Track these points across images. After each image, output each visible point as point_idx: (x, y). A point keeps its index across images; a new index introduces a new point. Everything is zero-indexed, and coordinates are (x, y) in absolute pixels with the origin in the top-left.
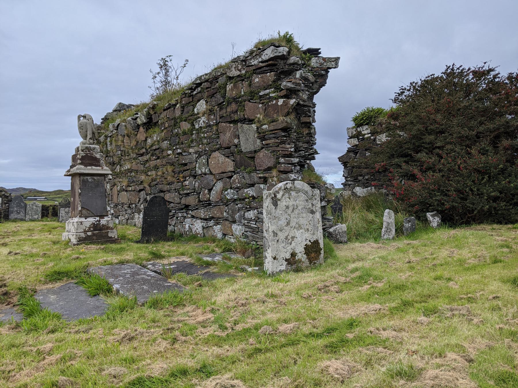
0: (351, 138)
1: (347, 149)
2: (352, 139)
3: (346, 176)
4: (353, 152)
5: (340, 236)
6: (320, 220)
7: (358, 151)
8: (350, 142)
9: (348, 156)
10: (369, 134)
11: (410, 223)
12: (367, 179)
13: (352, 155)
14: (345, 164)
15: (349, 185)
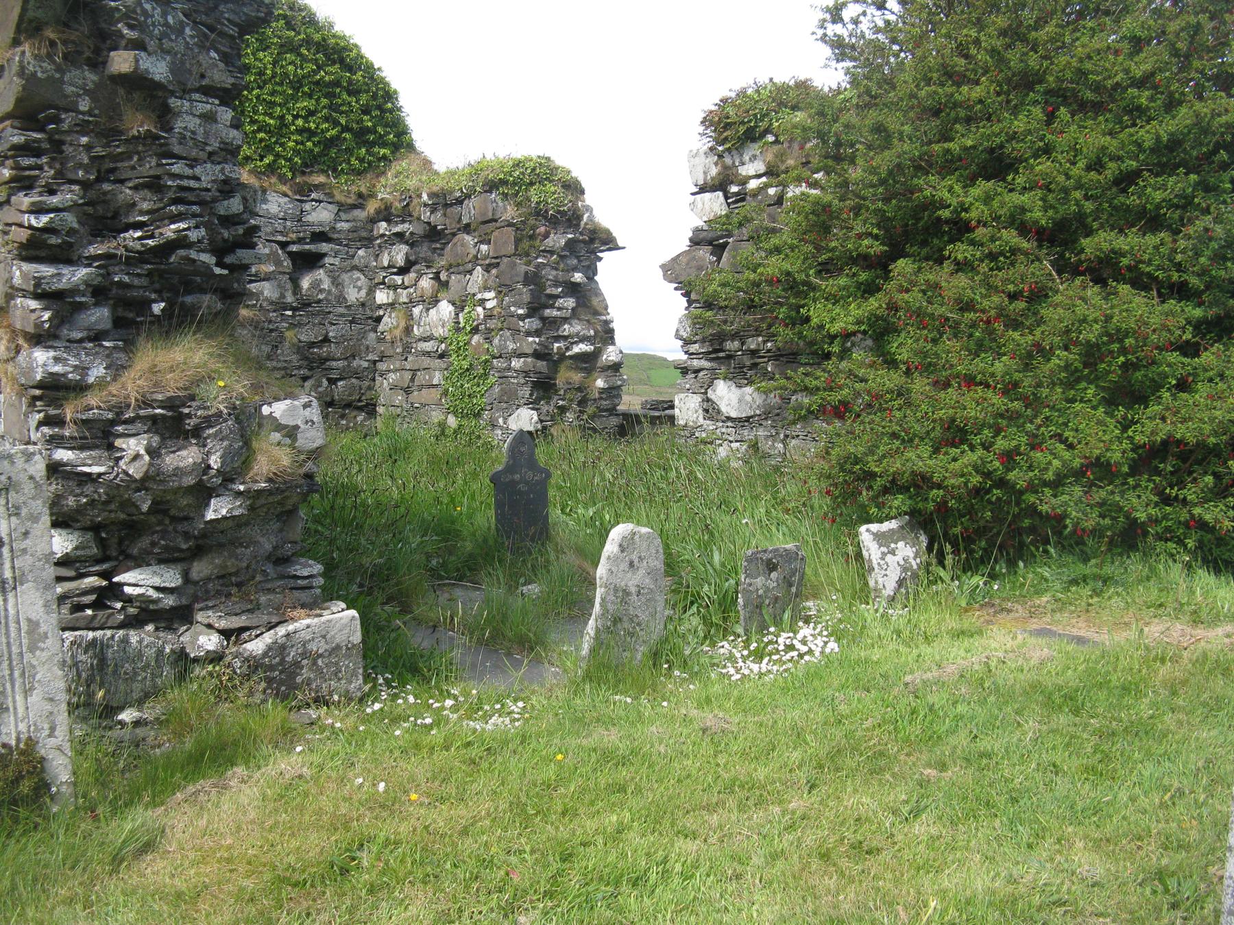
0: (703, 189)
1: (691, 234)
2: (707, 196)
3: (685, 335)
4: (710, 243)
5: (319, 671)
6: (43, 628)
7: (727, 244)
8: (700, 205)
9: (694, 257)
10: (759, 176)
11: (774, 575)
12: (754, 353)
13: (705, 254)
14: (687, 289)
15: (697, 371)
